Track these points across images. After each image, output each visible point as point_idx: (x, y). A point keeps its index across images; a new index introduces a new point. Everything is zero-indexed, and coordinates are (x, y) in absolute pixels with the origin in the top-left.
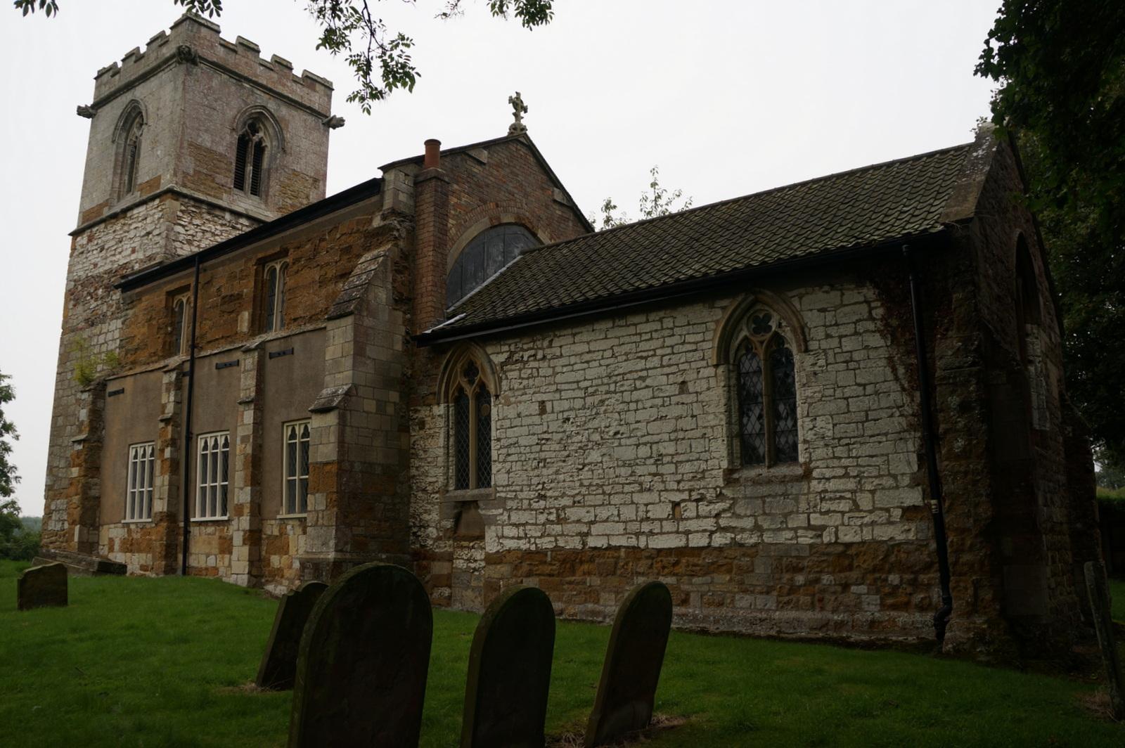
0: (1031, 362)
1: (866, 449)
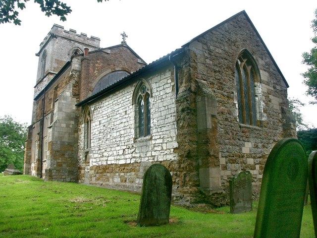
0: (256, 96)
1: (164, 129)
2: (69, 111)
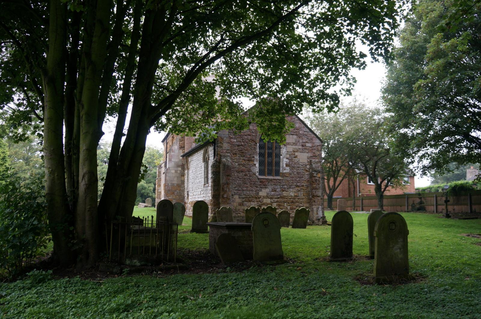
2: (177, 160)
